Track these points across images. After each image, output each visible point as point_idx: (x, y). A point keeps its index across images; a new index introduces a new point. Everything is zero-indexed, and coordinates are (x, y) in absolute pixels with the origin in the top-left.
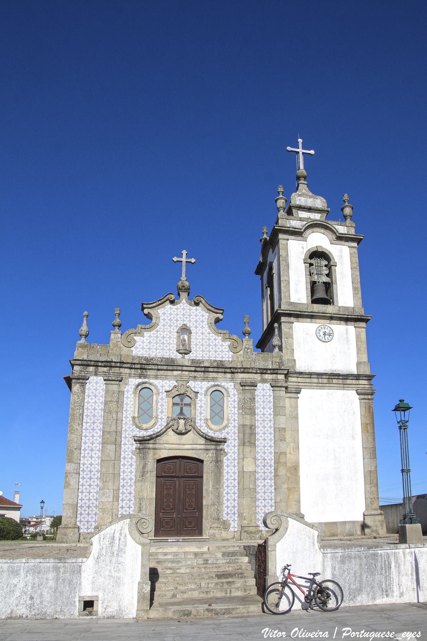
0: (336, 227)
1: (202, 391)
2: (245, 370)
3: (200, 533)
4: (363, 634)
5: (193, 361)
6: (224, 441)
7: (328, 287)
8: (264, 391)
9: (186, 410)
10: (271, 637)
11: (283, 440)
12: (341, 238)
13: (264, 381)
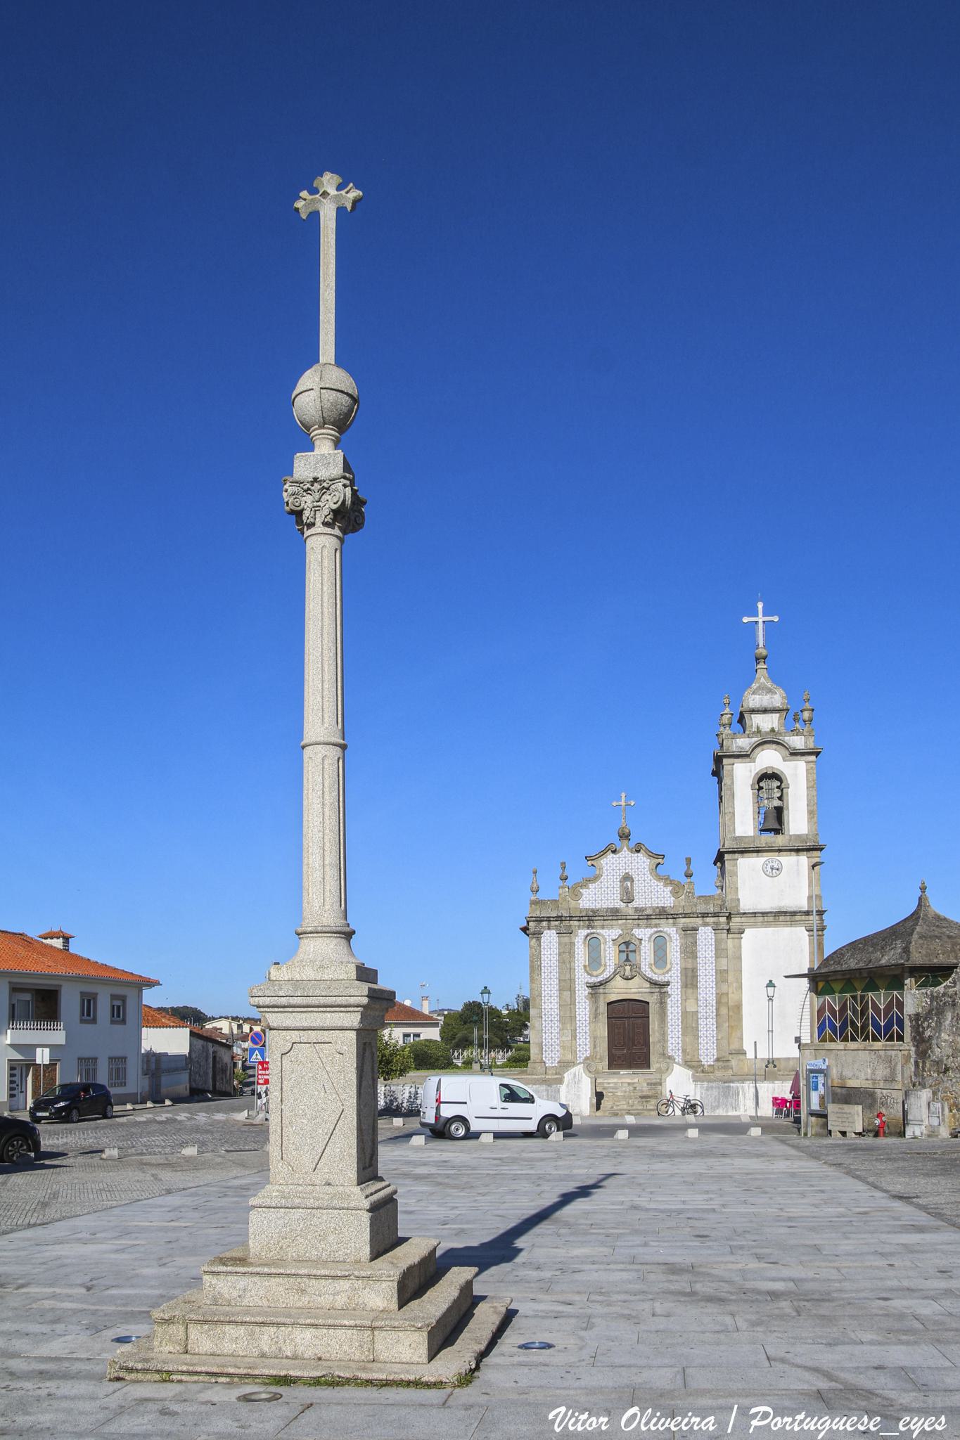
0: (786, 738)
1: (646, 938)
2: (686, 916)
3: (649, 1067)
4: (802, 1422)
5: (636, 909)
6: (668, 984)
7: (779, 811)
8: (706, 935)
9: (631, 956)
10: (571, 1428)
11: (725, 981)
12: (795, 754)
13: (705, 924)
